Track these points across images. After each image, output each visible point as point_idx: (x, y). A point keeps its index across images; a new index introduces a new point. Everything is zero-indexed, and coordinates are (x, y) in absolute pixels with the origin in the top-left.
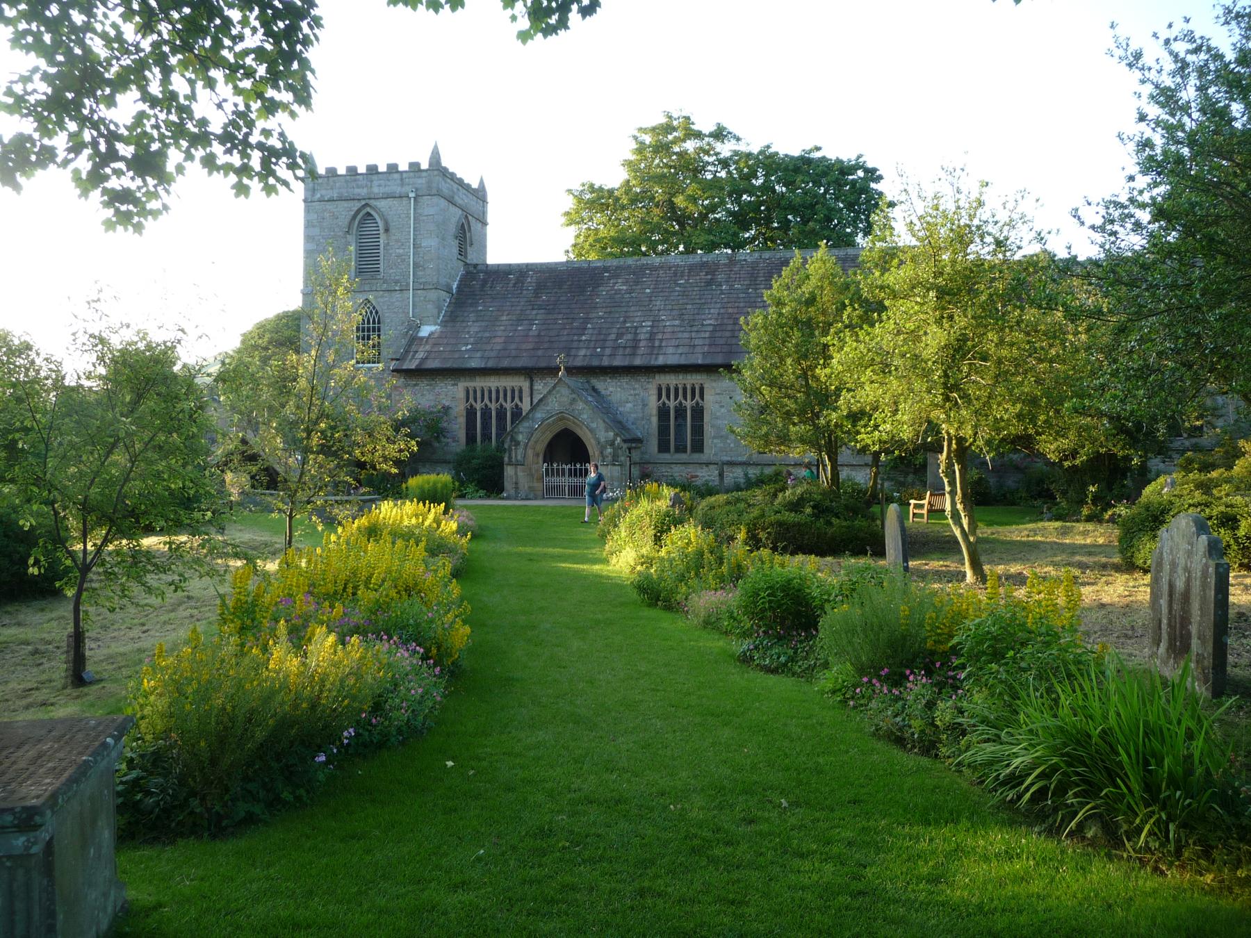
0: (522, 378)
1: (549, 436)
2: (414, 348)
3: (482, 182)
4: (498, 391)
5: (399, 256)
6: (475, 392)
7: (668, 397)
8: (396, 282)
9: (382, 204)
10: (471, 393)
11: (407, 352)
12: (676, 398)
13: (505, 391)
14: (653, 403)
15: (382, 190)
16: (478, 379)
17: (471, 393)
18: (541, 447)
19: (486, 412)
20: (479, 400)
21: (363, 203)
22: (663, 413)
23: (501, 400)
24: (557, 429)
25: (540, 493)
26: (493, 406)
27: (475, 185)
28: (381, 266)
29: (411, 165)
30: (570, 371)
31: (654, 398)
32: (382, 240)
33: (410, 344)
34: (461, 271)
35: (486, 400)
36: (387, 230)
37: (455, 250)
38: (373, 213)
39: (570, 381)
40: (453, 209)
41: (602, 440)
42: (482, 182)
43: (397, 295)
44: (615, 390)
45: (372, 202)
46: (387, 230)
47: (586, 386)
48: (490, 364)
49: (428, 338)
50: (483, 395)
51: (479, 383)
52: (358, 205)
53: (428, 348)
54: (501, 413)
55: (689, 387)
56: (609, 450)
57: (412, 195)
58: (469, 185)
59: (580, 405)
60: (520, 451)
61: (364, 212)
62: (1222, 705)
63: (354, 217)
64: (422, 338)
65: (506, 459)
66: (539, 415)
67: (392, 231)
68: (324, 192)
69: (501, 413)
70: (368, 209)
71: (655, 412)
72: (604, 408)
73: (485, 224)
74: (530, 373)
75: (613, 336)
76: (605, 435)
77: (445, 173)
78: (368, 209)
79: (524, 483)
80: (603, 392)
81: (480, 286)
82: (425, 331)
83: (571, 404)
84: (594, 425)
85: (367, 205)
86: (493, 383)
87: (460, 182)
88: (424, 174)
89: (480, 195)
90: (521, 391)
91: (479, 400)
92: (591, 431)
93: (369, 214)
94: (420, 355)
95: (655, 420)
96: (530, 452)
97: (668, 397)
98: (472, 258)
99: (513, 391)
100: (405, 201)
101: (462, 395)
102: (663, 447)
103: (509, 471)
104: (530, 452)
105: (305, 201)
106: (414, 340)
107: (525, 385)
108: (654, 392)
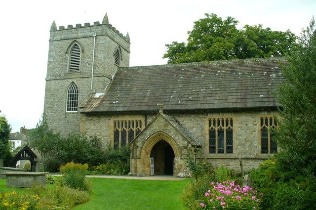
0: (141, 116)
1: (153, 144)
3: (128, 34)
4: (129, 123)
6: (119, 123)
7: (267, 124)
10: (117, 123)
12: (137, 126)
14: (207, 128)
17: (117, 123)
18: (149, 149)
20: (120, 127)
22: (212, 133)
23: (131, 127)
24: (157, 140)
25: (148, 173)
26: (127, 130)
27: (125, 35)
28: (80, 67)
29: (95, 23)
30: (168, 112)
33: (89, 101)
34: (116, 70)
35: (124, 127)
36: (83, 51)
37: (114, 61)
38: (77, 44)
40: (113, 43)
42: (128, 34)
43: (86, 79)
44: (188, 122)
45: (78, 40)
46: (83, 51)
50: (122, 124)
51: (121, 119)
54: (131, 133)
56: (185, 151)
60: (138, 151)
61: (74, 44)
64: (96, 98)
66: (148, 132)
68: (58, 37)
69: (131, 133)
70: (76, 43)
71: (208, 132)
74: (146, 114)
77: (110, 26)
78: (76, 43)
80: (181, 123)
81: (124, 77)
82: (97, 95)
83: (165, 127)
86: (127, 119)
90: (141, 122)
91: (120, 127)
93: (76, 45)
96: (143, 152)
97: (267, 124)
98: (122, 64)
99: (137, 122)
100: (91, 38)
101: (112, 124)
102: (212, 150)
104: (143, 152)
105: (50, 41)
106: (91, 99)
107: (143, 119)
108: (208, 122)
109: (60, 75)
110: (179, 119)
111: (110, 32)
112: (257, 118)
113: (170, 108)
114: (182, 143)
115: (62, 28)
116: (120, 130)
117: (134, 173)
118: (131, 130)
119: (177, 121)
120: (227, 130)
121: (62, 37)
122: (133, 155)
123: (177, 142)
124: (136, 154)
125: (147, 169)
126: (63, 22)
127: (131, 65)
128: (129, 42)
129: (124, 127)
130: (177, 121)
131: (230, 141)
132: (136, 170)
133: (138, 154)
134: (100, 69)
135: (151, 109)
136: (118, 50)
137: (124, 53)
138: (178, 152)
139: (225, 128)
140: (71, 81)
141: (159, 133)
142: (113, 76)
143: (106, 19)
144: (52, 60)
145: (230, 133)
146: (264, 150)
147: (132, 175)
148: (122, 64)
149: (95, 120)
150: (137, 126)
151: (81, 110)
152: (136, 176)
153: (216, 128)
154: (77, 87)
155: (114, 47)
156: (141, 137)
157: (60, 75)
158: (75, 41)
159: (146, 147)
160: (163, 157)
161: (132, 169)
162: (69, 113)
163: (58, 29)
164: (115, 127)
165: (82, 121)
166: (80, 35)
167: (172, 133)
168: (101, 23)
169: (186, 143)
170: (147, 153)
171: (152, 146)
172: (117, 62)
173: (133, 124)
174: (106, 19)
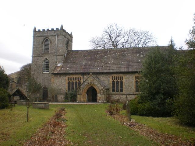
1: (87, 88)
3: (71, 33)
6: (70, 78)
8: (53, 54)
9: (50, 37)
10: (137, 77)
11: (55, 69)
12: (79, 80)
13: (70, 78)
14: (111, 80)
15: (51, 34)
17: (137, 77)
18: (86, 91)
19: (73, 83)
20: (71, 80)
21: (46, 37)
22: (113, 83)
24: (89, 87)
25: (85, 101)
26: (74, 81)
31: (111, 79)
33: (55, 68)
35: (76, 80)
37: (66, 47)
40: (65, 38)
41: (100, 89)
42: (71, 33)
43: (53, 57)
44: (103, 78)
45: (48, 37)
46: (51, 43)
51: (71, 76)
52: (45, 37)
55: (119, 77)
57: (57, 35)
58: (69, 34)
63: (44, 40)
69: (80, 83)
71: (111, 83)
72: (100, 82)
73: (72, 42)
74: (83, 74)
76: (101, 88)
77: (65, 31)
79: (82, 99)
82: (59, 65)
85: (46, 38)
86: (74, 76)
87: (67, 33)
89: (71, 36)
90: (81, 78)
91: (71, 80)
93: (47, 39)
94: (58, 70)
95: (111, 84)
97: (114, 79)
102: (113, 90)
103: (78, 96)
105: (33, 37)
106: (56, 67)
110: (99, 77)
111: (64, 34)
112: (66, 78)
114: (101, 88)
115: (39, 30)
118: (76, 81)
119: (97, 78)
121: (40, 35)
123: (98, 87)
126: (40, 28)
127: (73, 49)
129: (76, 80)
130: (97, 78)
131: (121, 87)
132: (80, 100)
136: (67, 42)
137: (70, 42)
139: (119, 81)
140: (45, 57)
141: (91, 83)
143: (62, 27)
144: (35, 46)
145: (121, 83)
147: (78, 102)
149: (58, 76)
150: (79, 80)
151: (52, 72)
153: (115, 81)
154: (48, 61)
155: (66, 40)
157: (39, 55)
158: (46, 38)
160: (92, 95)
162: (44, 73)
163: (37, 30)
164: (112, 80)
165: (52, 77)
169: (102, 88)
170: (85, 92)
171: (97, 91)
172: (67, 48)
173: (77, 79)
174: (62, 27)
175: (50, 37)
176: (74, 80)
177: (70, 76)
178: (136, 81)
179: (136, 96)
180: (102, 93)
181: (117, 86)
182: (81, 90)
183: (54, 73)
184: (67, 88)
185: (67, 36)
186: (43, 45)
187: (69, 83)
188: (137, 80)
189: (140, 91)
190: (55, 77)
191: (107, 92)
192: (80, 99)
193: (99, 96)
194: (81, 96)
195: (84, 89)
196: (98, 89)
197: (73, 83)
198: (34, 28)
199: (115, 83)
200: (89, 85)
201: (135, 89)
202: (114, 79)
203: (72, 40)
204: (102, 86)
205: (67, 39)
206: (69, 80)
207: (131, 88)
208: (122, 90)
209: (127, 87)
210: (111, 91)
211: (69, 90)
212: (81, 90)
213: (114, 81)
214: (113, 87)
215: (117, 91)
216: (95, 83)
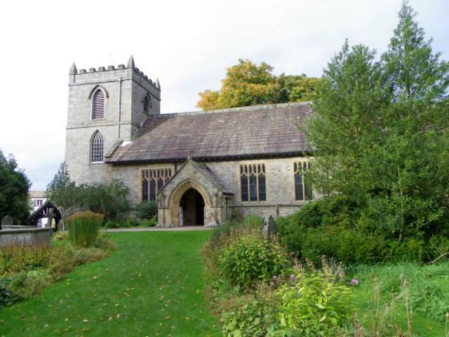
2: (117, 152)
5: (113, 109)
9: (106, 85)
12: (166, 175)
16: (149, 166)
19: (153, 182)
24: (186, 189)
25: (177, 224)
26: (156, 179)
27: (154, 81)
31: (239, 172)
32: (106, 100)
33: (115, 150)
35: (153, 177)
36: (108, 97)
38: (101, 89)
39: (194, 163)
41: (211, 193)
46: (108, 97)
47: (203, 167)
48: (154, 158)
49: (125, 147)
51: (149, 168)
52: (94, 86)
53: (125, 151)
57: (119, 80)
59: (199, 174)
62: (137, 225)
63: (92, 92)
64: (122, 148)
65: (159, 206)
66: (177, 181)
67: (110, 97)
69: (160, 182)
70: (99, 88)
71: (239, 179)
73: (159, 100)
75: (217, 143)
76: (213, 190)
78: (99, 88)
84: (206, 185)
86: (156, 167)
88: (126, 70)
92: (205, 188)
93: (99, 90)
94: (120, 155)
95: (239, 184)
100: (116, 83)
101: (140, 174)
102: (244, 198)
103: (160, 212)
109: (83, 123)
110: (208, 165)
113: (199, 155)
116: (149, 180)
117: (162, 224)
120: (250, 177)
121: (84, 82)
122: (161, 205)
123: (207, 189)
124: (164, 203)
125: (176, 220)
127: (161, 113)
128: (159, 90)
129: (153, 177)
130: (208, 169)
131: (263, 188)
133: (166, 204)
134: (127, 116)
135: (181, 156)
136: (146, 98)
137: (153, 100)
138: (208, 201)
139: (257, 175)
140: (95, 129)
141: (188, 181)
142: (141, 125)
145: (262, 180)
146: (299, 197)
147: (160, 227)
148: (151, 112)
152: (164, 227)
153: (248, 175)
156: (169, 186)
157: (83, 123)
158: (98, 86)
159: (175, 196)
161: (160, 220)
162: (93, 164)
164: (143, 177)
166: (103, 79)
167: (201, 180)
168: (126, 66)
169: (216, 190)
170: (176, 203)
171: (204, 197)
172: (146, 109)
173: (162, 174)
175: (106, 85)
176: (147, 176)
177: (146, 168)
178: (295, 175)
179: (298, 209)
180: (214, 204)
181: (253, 187)
182: (165, 197)
183: (112, 160)
184: (140, 195)
185: (145, 84)
186: (91, 102)
187: (145, 183)
188: (298, 173)
189: (306, 199)
190: (113, 170)
191: (231, 203)
192: (164, 219)
193: (208, 210)
194: (166, 210)
195: (171, 192)
196: (207, 195)
197: (153, 182)
198: (71, 64)
199: (149, 183)
200: (184, 185)
201: (294, 194)
202: (246, 171)
203: (159, 95)
204: (215, 186)
205: (144, 91)
206: (146, 177)
207: (284, 192)
208: (263, 197)
209: (276, 190)
210: (239, 197)
211: (145, 197)
212: (165, 197)
213: (244, 175)
214: (244, 189)
215: (253, 199)
216: (199, 179)
